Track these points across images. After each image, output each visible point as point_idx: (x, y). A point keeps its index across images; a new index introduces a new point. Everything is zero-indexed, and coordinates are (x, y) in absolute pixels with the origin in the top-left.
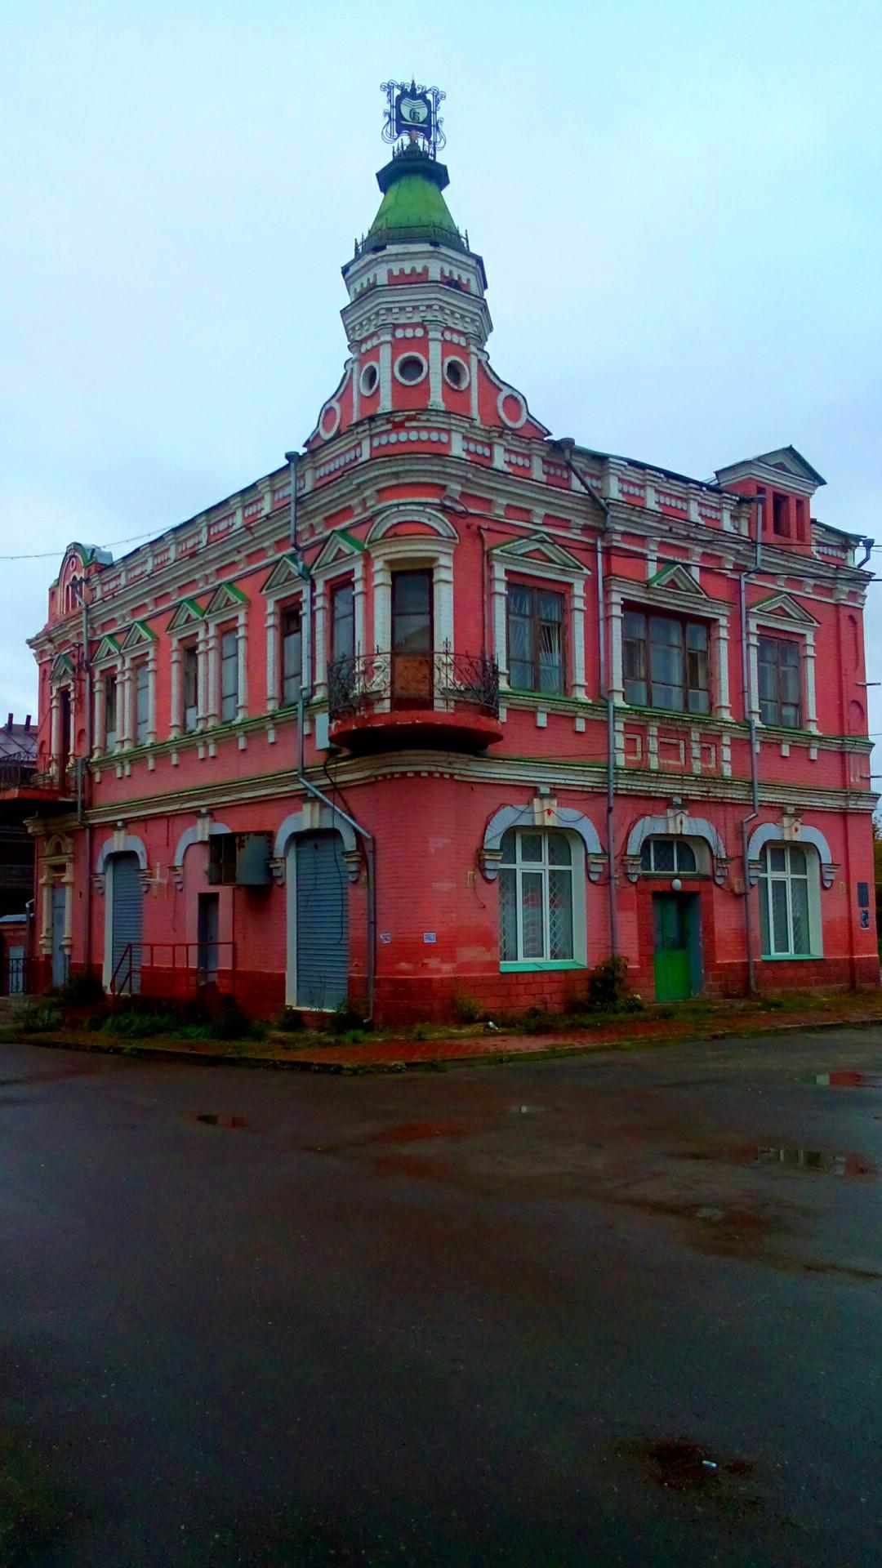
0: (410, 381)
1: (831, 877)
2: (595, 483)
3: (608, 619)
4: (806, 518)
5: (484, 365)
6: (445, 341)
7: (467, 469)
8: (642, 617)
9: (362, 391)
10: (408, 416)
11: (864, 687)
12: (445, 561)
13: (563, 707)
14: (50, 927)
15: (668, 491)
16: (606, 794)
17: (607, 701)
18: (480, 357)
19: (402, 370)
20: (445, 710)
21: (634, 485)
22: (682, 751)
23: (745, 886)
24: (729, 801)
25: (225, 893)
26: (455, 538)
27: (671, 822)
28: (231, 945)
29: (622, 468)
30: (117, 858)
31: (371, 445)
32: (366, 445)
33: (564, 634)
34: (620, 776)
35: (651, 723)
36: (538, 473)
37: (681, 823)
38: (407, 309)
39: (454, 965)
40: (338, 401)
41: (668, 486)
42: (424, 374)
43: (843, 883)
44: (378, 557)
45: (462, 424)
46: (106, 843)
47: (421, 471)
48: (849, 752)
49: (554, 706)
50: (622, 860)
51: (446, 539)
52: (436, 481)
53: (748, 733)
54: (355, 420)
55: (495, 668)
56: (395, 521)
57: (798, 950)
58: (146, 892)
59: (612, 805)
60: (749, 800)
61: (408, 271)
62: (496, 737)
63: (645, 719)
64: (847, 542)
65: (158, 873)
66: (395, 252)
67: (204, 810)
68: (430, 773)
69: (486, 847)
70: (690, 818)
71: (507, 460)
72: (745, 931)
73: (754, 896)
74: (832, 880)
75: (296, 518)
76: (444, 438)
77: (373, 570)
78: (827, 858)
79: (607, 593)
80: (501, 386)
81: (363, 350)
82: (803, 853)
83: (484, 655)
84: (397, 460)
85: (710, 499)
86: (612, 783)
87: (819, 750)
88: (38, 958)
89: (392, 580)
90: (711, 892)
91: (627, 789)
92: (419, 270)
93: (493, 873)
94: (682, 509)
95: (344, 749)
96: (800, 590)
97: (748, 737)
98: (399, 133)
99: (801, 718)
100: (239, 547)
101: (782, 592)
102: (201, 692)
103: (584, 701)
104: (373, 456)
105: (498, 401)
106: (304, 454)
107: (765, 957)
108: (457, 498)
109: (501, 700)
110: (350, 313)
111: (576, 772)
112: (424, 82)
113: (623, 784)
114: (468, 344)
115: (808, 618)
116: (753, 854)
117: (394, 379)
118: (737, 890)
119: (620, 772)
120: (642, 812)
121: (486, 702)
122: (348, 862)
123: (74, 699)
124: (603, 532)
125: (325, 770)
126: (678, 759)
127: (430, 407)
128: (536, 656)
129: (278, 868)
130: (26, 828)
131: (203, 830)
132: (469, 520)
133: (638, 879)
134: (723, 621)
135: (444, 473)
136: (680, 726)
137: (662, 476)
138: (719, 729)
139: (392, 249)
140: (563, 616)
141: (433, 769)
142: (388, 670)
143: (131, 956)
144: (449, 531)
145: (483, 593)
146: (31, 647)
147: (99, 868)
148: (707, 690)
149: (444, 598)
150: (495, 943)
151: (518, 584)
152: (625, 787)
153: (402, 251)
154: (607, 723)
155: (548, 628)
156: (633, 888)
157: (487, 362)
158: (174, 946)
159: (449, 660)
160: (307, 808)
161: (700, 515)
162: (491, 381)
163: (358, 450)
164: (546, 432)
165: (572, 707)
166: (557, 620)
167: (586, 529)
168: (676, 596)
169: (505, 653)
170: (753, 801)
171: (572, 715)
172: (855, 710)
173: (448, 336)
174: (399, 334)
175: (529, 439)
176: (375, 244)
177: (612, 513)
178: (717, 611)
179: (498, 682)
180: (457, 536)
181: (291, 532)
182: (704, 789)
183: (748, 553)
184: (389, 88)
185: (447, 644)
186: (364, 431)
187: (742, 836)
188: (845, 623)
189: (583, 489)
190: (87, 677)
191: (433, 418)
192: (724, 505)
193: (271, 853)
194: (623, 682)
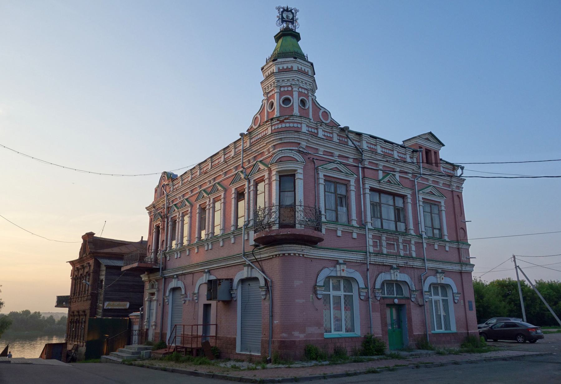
1: (458, 298)
2: (357, 143)
3: (364, 194)
4: (438, 158)
5: (314, 100)
6: (299, 91)
7: (309, 137)
8: (378, 194)
9: (268, 110)
11: (465, 222)
12: (300, 171)
13: (348, 228)
14: (148, 317)
15: (386, 147)
16: (366, 263)
17: (365, 226)
18: (313, 98)
19: (283, 102)
20: (300, 228)
22: (396, 246)
23: (424, 302)
24: (415, 267)
25: (213, 303)
26: (304, 162)
27: (393, 275)
29: (368, 138)
30: (175, 290)
31: (271, 129)
32: (270, 128)
33: (347, 200)
34: (371, 256)
35: (383, 235)
36: (336, 138)
38: (285, 81)
39: (305, 335)
40: (259, 114)
41: (385, 145)
42: (291, 103)
43: (462, 301)
44: (273, 170)
47: (292, 137)
48: (461, 248)
49: (344, 228)
50: (373, 291)
51: (300, 163)
52: (296, 141)
53: (421, 240)
54: (266, 120)
55: (320, 212)
56: (280, 156)
57: (446, 329)
58: (184, 303)
59: (368, 268)
60: (423, 266)
62: (321, 240)
63: (380, 233)
64: (454, 167)
65: (188, 296)
66: (281, 61)
67: (206, 270)
68: (295, 254)
69: (318, 284)
72: (425, 321)
73: (427, 306)
74: (458, 300)
75: (243, 157)
76: (299, 126)
77: (272, 175)
78: (455, 290)
79: (364, 184)
80: (321, 108)
81: (269, 96)
82: (446, 289)
83: (316, 206)
84: (281, 133)
86: (368, 259)
87: (449, 247)
89: (280, 178)
90: (410, 304)
91: (374, 262)
93: (320, 295)
94: (391, 154)
95: (260, 245)
96: (438, 185)
97: (421, 242)
98: (282, 23)
99: (441, 234)
100: (222, 169)
101: (431, 186)
102: (207, 224)
103: (356, 226)
104: (272, 132)
106: (247, 134)
107: (433, 332)
108: (304, 147)
109: (322, 225)
110: (264, 83)
111: (354, 255)
112: (291, 6)
113: (373, 259)
114: (308, 93)
115: (442, 196)
116: (426, 288)
117: (280, 105)
118: (420, 304)
119: (372, 254)
120: (380, 271)
121: (316, 225)
122: (261, 291)
123: (161, 229)
125: (253, 253)
126: (394, 250)
128: (336, 208)
130: (142, 278)
131: (204, 278)
132: (309, 156)
133: (380, 299)
134: (409, 196)
135: (299, 138)
136: (395, 237)
137: (383, 141)
138: (410, 238)
139: (279, 60)
140: (347, 193)
141: (296, 252)
142: (278, 213)
143: (176, 329)
145: (315, 184)
146: (147, 210)
147: (167, 294)
149: (300, 184)
150: (322, 325)
151: (328, 179)
152: (373, 260)
153: (283, 61)
154: (366, 235)
155: (341, 197)
156: (378, 303)
157: (315, 99)
158: (192, 326)
159: (301, 208)
160: (246, 268)
161: (398, 156)
162: (317, 106)
163: (267, 131)
165: (310, 370)
166: (344, 194)
168: (390, 186)
169: (324, 207)
170: (425, 267)
171: (352, 231)
172: (462, 231)
173: (300, 90)
174: (282, 89)
175: (332, 127)
176: (274, 59)
177: (364, 154)
178: (406, 192)
179: (321, 217)
181: (241, 163)
182: (405, 262)
183: (417, 171)
184: (278, 9)
185: (300, 202)
186: (269, 124)
187: (421, 281)
188: (456, 198)
189: (353, 145)
190: (166, 220)
191: (294, 119)
192: (407, 153)
193: (232, 287)
194: (371, 219)
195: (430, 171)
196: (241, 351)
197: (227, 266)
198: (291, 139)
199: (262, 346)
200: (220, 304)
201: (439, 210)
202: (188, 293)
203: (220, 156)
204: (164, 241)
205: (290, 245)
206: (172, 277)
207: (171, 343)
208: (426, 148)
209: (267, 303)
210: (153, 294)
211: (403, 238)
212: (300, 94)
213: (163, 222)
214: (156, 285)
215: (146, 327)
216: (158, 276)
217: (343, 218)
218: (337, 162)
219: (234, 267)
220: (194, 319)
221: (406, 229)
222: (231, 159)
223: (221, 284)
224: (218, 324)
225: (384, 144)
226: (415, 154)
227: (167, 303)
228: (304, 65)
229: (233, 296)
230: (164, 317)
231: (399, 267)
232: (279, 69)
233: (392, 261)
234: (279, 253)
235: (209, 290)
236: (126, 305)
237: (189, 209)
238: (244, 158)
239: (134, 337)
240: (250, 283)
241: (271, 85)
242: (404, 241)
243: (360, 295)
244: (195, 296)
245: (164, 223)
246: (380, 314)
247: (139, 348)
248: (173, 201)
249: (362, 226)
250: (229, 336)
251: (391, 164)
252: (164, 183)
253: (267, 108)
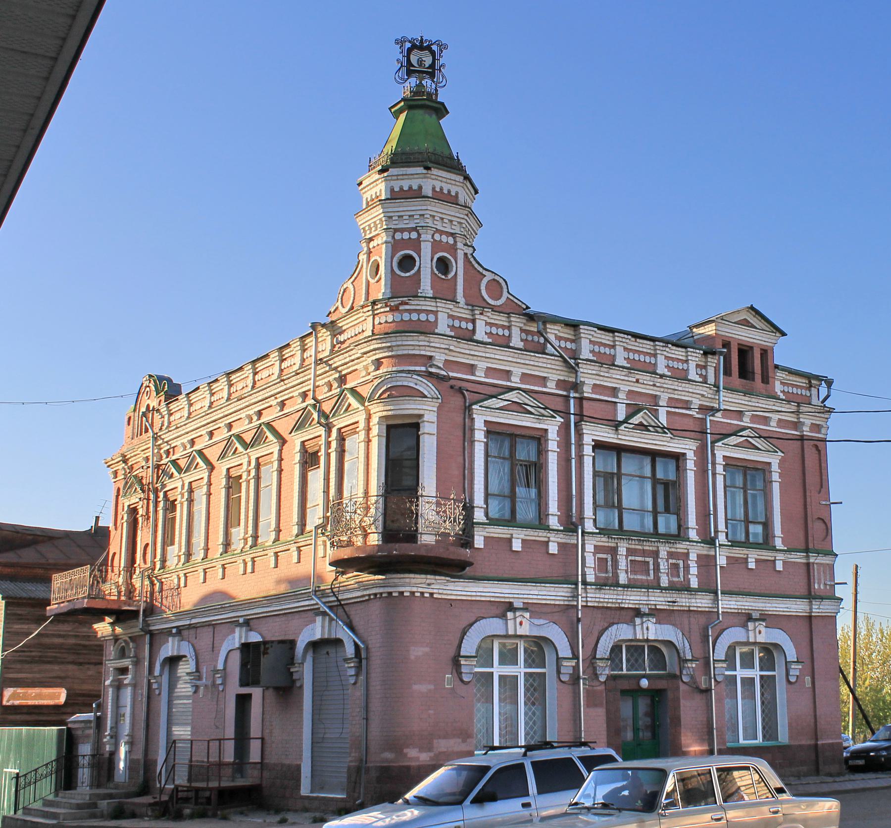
0: (405, 273)
5: (470, 257)
10: (402, 301)
21: (605, 345)
25: (256, 693)
27: (638, 628)
28: (260, 740)
33: (540, 472)
37: (647, 629)
39: (432, 754)
41: (637, 344)
42: (416, 268)
43: (808, 679)
45: (447, 306)
46: (162, 648)
47: (416, 345)
48: (813, 563)
52: (423, 353)
60: (714, 608)
61: (406, 188)
65: (204, 676)
67: (241, 620)
69: (462, 654)
70: (658, 625)
71: (488, 331)
75: (316, 376)
76: (432, 318)
79: (580, 435)
80: (484, 272)
85: (677, 353)
88: (103, 755)
90: (678, 688)
92: (415, 187)
93: (468, 675)
105: (482, 285)
112: (430, 36)
113: (595, 597)
120: (612, 621)
123: (142, 516)
124: (576, 386)
127: (419, 295)
129: (297, 671)
131: (238, 638)
133: (607, 680)
134: (690, 455)
138: (685, 547)
140: (539, 456)
141: (414, 589)
144: (433, 393)
147: (157, 672)
148: (763, 490)
151: (493, 431)
160: (319, 619)
164: (525, 307)
167: (560, 384)
172: (819, 525)
173: (437, 237)
174: (398, 236)
180: (439, 396)
181: (311, 387)
184: (400, 42)
193: (293, 658)
195: (744, 396)
196: (312, 792)
197: (283, 612)
198: (412, 348)
199: (348, 779)
200: (270, 693)
201: (764, 481)
202: (204, 670)
203: (272, 363)
204: (147, 545)
205: (402, 576)
206: (168, 632)
207: (163, 782)
208: (740, 342)
209: (360, 692)
210: (124, 671)
211: (668, 549)
212: (436, 246)
213: (145, 501)
214: (130, 649)
215: (108, 748)
216: (137, 629)
217: (527, 512)
218: (512, 396)
219: (297, 616)
220: (217, 727)
221: (679, 527)
222: (293, 376)
223: (269, 651)
224: (266, 738)
225: (633, 343)
226: (710, 358)
227: (157, 692)
228: (448, 181)
229: (294, 677)
230: (151, 724)
231: (654, 612)
232: (392, 190)
233: (638, 598)
234: (381, 590)
235: (244, 665)
236: (58, 697)
237: (205, 475)
238: (318, 378)
239: (80, 771)
240: (330, 651)
241: (376, 226)
242: (671, 555)
243: (559, 672)
244: (219, 676)
245: (148, 504)
246: (605, 710)
247: (93, 794)
248: (168, 453)
249: (571, 525)
250: (287, 762)
251: (648, 387)
252: (149, 402)
253: (367, 272)
